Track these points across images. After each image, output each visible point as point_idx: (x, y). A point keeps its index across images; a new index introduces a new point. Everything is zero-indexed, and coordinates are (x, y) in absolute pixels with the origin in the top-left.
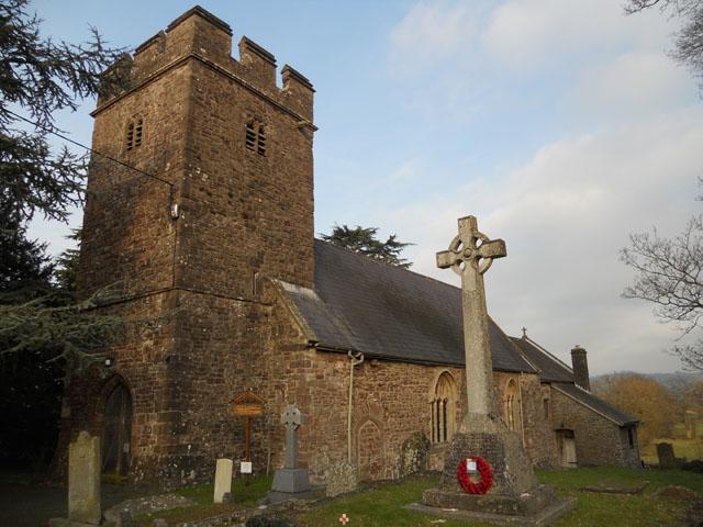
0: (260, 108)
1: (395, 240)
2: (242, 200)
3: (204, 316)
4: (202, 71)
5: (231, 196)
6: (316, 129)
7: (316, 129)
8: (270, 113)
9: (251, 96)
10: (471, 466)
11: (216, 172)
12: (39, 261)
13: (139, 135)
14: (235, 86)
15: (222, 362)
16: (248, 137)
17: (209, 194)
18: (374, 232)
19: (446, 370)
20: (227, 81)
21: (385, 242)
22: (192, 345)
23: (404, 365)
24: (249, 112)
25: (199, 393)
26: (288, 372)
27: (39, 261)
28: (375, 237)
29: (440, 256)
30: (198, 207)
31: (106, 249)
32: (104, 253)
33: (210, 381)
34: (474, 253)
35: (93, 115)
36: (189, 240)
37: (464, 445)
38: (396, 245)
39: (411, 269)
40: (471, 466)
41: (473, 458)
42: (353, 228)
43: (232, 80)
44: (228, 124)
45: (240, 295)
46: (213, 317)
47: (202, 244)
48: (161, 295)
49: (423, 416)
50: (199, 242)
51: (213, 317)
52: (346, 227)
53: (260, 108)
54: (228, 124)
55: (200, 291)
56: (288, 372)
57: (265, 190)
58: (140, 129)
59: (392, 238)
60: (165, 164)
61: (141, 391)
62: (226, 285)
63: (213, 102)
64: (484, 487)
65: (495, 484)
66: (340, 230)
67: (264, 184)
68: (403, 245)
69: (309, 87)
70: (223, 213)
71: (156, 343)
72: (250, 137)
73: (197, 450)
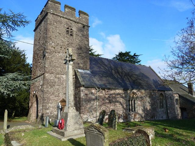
0: (70, 23)
2: (65, 49)
3: (53, 80)
4: (51, 16)
5: (61, 48)
6: (89, 27)
7: (89, 27)
8: (73, 23)
9: (67, 20)
11: (57, 42)
12: (90, 48)
14: (62, 18)
15: (59, 91)
16: (67, 32)
17: (54, 48)
18: (130, 53)
20: (59, 17)
22: (49, 88)
24: (67, 25)
25: (52, 99)
27: (90, 48)
28: (130, 54)
30: (51, 52)
33: (55, 96)
36: (48, 61)
39: (102, 56)
42: (124, 52)
43: (61, 17)
44: (60, 29)
45: (65, 74)
46: (56, 80)
47: (52, 61)
50: (52, 61)
51: (56, 80)
52: (122, 52)
53: (70, 23)
54: (60, 29)
55: (52, 73)
57: (73, 45)
59: (135, 54)
62: (60, 71)
63: (55, 23)
67: (72, 44)
68: (138, 56)
69: (87, 15)
70: (59, 53)
72: (68, 32)
73: (52, 114)
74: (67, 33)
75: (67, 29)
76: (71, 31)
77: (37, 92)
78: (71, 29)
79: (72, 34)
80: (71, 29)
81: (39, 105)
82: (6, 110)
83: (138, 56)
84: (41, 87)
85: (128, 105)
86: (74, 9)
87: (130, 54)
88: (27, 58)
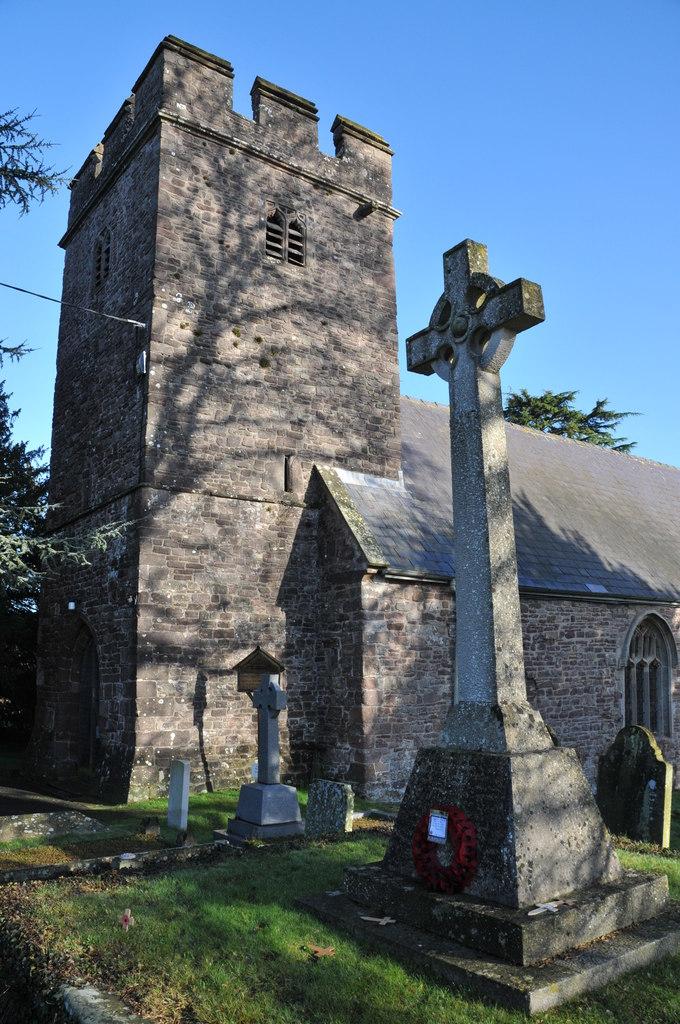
1: (606, 408)
10: (438, 828)
13: (107, 260)
18: (570, 398)
19: (650, 612)
21: (589, 412)
23: (566, 605)
26: (342, 618)
28: (573, 406)
29: (415, 344)
31: (74, 438)
32: (72, 444)
34: (472, 323)
35: (62, 244)
37: (437, 776)
38: (606, 416)
40: (438, 828)
41: (443, 808)
42: (536, 393)
48: (127, 498)
49: (608, 690)
52: (524, 393)
56: (342, 618)
58: (108, 251)
59: (600, 404)
60: (133, 295)
61: (108, 649)
64: (455, 882)
65: (481, 873)
66: (516, 397)
68: (616, 416)
71: (121, 575)
74: (268, 247)
75: (270, 225)
76: (292, 236)
77: (91, 604)
78: (294, 226)
79: (296, 252)
80: (294, 226)
81: (103, 684)
82: (529, 914)
83: (616, 416)
84: (114, 574)
85: (623, 691)
86: (309, 111)
87: (570, 403)
88: (16, 414)
